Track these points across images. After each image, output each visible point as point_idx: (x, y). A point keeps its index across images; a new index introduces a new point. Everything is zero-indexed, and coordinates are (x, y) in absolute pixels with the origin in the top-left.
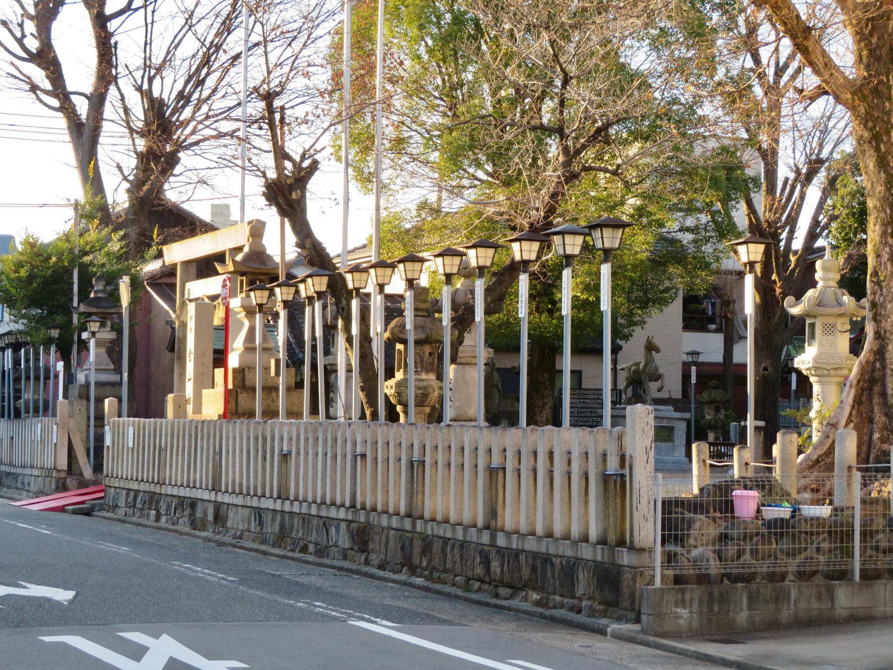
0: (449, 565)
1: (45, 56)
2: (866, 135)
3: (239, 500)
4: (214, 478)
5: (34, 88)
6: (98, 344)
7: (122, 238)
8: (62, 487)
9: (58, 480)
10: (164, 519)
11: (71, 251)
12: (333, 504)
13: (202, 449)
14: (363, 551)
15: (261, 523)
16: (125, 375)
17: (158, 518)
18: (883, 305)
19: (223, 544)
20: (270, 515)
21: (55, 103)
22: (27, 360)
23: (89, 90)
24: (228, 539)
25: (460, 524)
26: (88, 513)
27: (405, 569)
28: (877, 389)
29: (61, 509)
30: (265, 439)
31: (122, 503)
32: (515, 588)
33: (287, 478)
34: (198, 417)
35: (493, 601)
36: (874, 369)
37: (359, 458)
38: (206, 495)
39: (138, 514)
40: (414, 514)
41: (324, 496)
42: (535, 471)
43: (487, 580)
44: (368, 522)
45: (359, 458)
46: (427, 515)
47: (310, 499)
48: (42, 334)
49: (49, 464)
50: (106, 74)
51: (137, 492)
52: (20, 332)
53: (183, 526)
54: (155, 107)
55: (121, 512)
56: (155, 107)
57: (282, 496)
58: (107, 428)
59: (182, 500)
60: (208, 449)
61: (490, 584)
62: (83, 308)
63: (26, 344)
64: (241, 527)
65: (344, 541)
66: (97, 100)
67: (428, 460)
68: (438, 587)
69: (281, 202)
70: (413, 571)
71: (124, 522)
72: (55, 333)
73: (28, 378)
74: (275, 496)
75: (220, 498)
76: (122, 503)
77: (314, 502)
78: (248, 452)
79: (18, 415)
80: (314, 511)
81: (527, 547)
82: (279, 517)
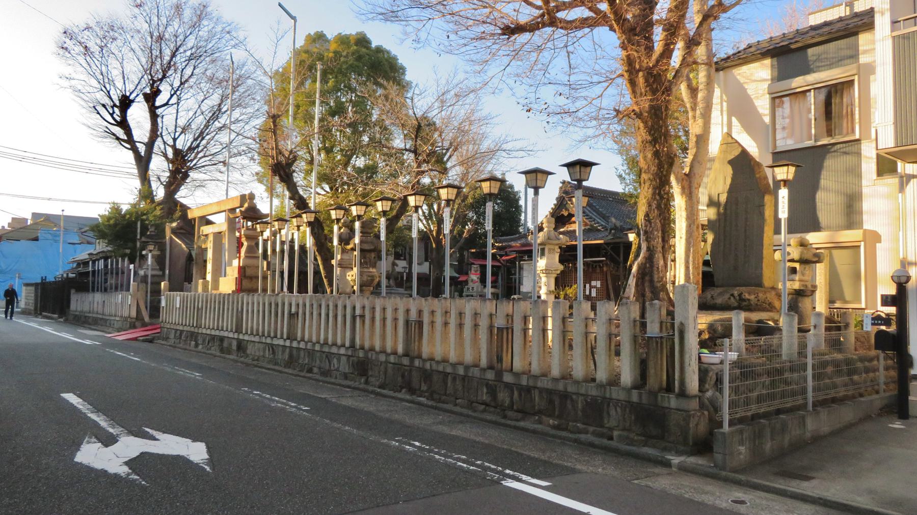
0: (450, 390)
1: (123, 123)
2: (649, 138)
3: (257, 339)
4: (237, 326)
5: (118, 138)
6: (153, 257)
7: (162, 209)
8: (133, 326)
9: (131, 323)
10: (200, 347)
11: (137, 213)
12: (335, 344)
13: (228, 309)
14: (362, 375)
15: (274, 352)
16: (167, 272)
17: (197, 345)
18: (651, 232)
19: (247, 365)
20: (281, 348)
21: (128, 146)
22: (112, 265)
23: (146, 140)
24: (250, 361)
25: (460, 364)
26: (151, 341)
27: (404, 390)
28: (647, 278)
29: (135, 339)
30: (277, 305)
31: (172, 336)
32: (525, 413)
33: (295, 328)
34: (214, 292)
35: (503, 421)
36: (645, 267)
37: (358, 318)
38: (231, 335)
39: (182, 343)
40: (411, 354)
41: (326, 339)
42: (320, 314)
43: (493, 404)
44: (366, 357)
45: (358, 318)
46: (424, 356)
47: (314, 339)
48: (121, 251)
49: (126, 314)
50: (155, 133)
51: (182, 331)
52: (109, 251)
53: (215, 350)
54: (177, 152)
55: (171, 342)
56: (177, 152)
57: (291, 337)
58: (163, 297)
59: (213, 338)
60: (233, 309)
61: (495, 407)
62: (143, 239)
63: (111, 257)
64: (257, 354)
65: (344, 367)
66: (150, 145)
67: (426, 319)
68: (440, 405)
69: (282, 173)
70: (412, 391)
71: (175, 347)
72: (128, 251)
73: (112, 273)
74: (285, 337)
75: (241, 337)
76: (172, 336)
77: (318, 342)
78: (264, 312)
79: (106, 290)
80: (317, 348)
81: (539, 384)
82: (288, 350)
